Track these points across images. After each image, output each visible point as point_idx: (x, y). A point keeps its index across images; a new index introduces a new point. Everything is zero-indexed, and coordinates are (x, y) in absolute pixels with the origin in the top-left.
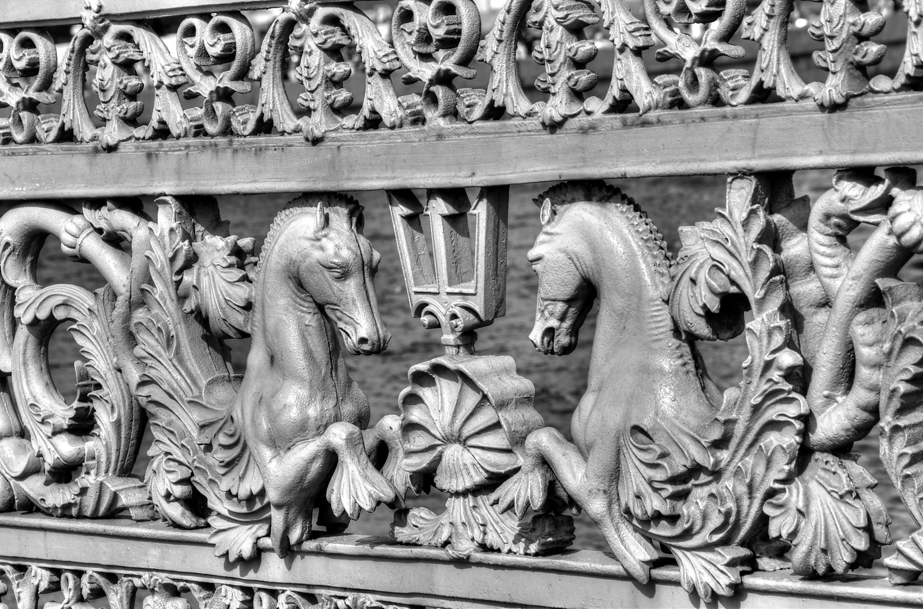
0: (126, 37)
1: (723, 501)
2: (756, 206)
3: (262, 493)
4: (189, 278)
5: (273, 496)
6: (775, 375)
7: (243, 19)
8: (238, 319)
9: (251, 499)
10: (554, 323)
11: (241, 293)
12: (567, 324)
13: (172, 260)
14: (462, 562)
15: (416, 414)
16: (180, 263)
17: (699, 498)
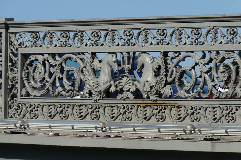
0: (52, 34)
1: (156, 89)
2: (213, 97)
3: (101, 90)
4: (93, 63)
5: (102, 90)
6: (163, 75)
7: (39, 33)
8: (99, 69)
9: (99, 92)
10: (139, 69)
11: (100, 66)
12: (140, 69)
13: (90, 61)
14: (125, 100)
15: (121, 81)
16: (91, 62)
17: (153, 89)
